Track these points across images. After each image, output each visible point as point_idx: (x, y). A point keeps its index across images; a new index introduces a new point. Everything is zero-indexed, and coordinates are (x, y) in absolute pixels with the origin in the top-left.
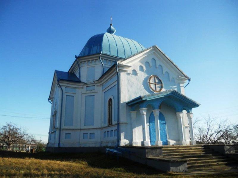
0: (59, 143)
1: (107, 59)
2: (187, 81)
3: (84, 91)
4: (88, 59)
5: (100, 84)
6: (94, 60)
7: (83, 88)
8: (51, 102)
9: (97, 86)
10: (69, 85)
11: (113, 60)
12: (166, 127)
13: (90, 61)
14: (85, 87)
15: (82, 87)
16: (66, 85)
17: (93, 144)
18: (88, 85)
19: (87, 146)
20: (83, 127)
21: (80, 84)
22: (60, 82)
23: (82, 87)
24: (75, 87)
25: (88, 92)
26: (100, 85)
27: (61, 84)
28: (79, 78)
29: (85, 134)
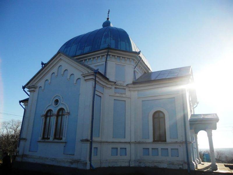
4: (98, 54)
6: (99, 57)
7: (111, 88)
11: (127, 57)
12: (11, 162)
13: (91, 59)
14: (113, 87)
15: (110, 86)
17: (126, 162)
18: (117, 87)
19: (119, 165)
25: (117, 95)
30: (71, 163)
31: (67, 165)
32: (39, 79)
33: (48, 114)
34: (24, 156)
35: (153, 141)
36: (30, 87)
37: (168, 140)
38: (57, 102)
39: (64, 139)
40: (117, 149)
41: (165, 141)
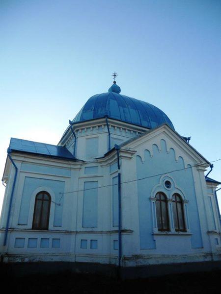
0: (75, 259)
1: (130, 129)
2: (209, 169)
3: (82, 173)
4: (94, 124)
5: (107, 163)
6: (90, 128)
7: (80, 169)
8: (5, 184)
9: (101, 166)
10: (26, 160)
13: (84, 129)
14: (83, 167)
15: (79, 167)
16: (22, 159)
20: (80, 229)
21: (77, 163)
22: (12, 154)
23: (79, 167)
24: (71, 168)
26: (107, 165)
27: (13, 158)
28: (74, 153)
29: (93, 241)
30: (205, 256)
31: (201, 260)
32: (186, 150)
33: (162, 198)
34: (136, 257)
35: (32, 229)
36: (129, 152)
37: (51, 227)
38: (168, 184)
39: (189, 231)
40: (93, 240)
41: (47, 228)
